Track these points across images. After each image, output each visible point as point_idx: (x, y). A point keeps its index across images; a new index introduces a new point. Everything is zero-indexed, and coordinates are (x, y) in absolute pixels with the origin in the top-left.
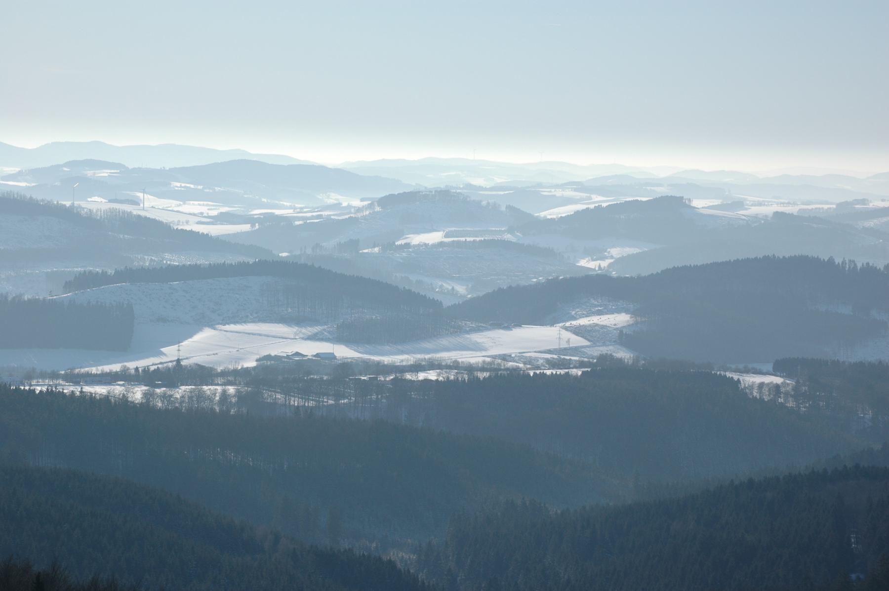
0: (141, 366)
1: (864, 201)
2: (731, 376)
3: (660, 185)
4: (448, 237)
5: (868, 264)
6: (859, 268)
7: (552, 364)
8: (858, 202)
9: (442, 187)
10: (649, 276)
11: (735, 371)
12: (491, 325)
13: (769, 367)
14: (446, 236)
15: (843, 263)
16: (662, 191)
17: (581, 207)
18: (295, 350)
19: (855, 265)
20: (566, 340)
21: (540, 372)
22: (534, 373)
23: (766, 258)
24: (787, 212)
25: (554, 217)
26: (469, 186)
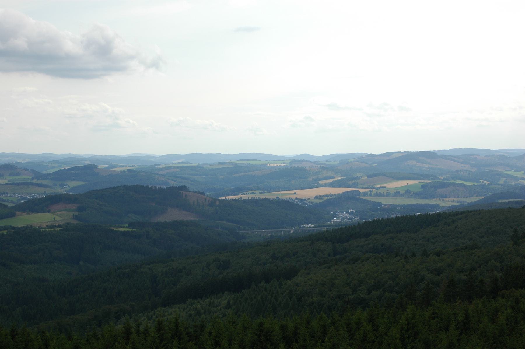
0: (385, 203)
1: (159, 165)
2: (113, 229)
3: (86, 161)
4: (10, 181)
5: (160, 187)
6: (157, 189)
7: (48, 227)
8: (155, 165)
9: (7, 163)
10: (239, 154)
11: (115, 227)
12: (26, 213)
13: (127, 225)
14: (9, 181)
15: (152, 187)
16: (87, 163)
17: (58, 169)
18: (15, 178)
19: (156, 187)
20: (53, 218)
21: (49, 230)
22: (42, 230)
23: (253, 153)
24: (132, 169)
25: (48, 173)
26: (17, 162)
